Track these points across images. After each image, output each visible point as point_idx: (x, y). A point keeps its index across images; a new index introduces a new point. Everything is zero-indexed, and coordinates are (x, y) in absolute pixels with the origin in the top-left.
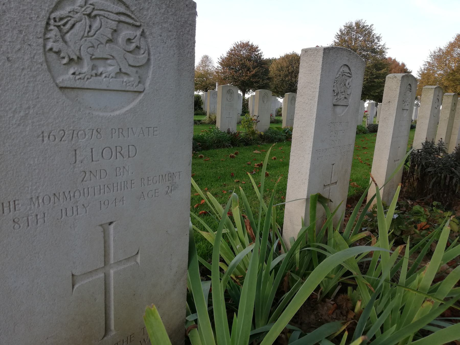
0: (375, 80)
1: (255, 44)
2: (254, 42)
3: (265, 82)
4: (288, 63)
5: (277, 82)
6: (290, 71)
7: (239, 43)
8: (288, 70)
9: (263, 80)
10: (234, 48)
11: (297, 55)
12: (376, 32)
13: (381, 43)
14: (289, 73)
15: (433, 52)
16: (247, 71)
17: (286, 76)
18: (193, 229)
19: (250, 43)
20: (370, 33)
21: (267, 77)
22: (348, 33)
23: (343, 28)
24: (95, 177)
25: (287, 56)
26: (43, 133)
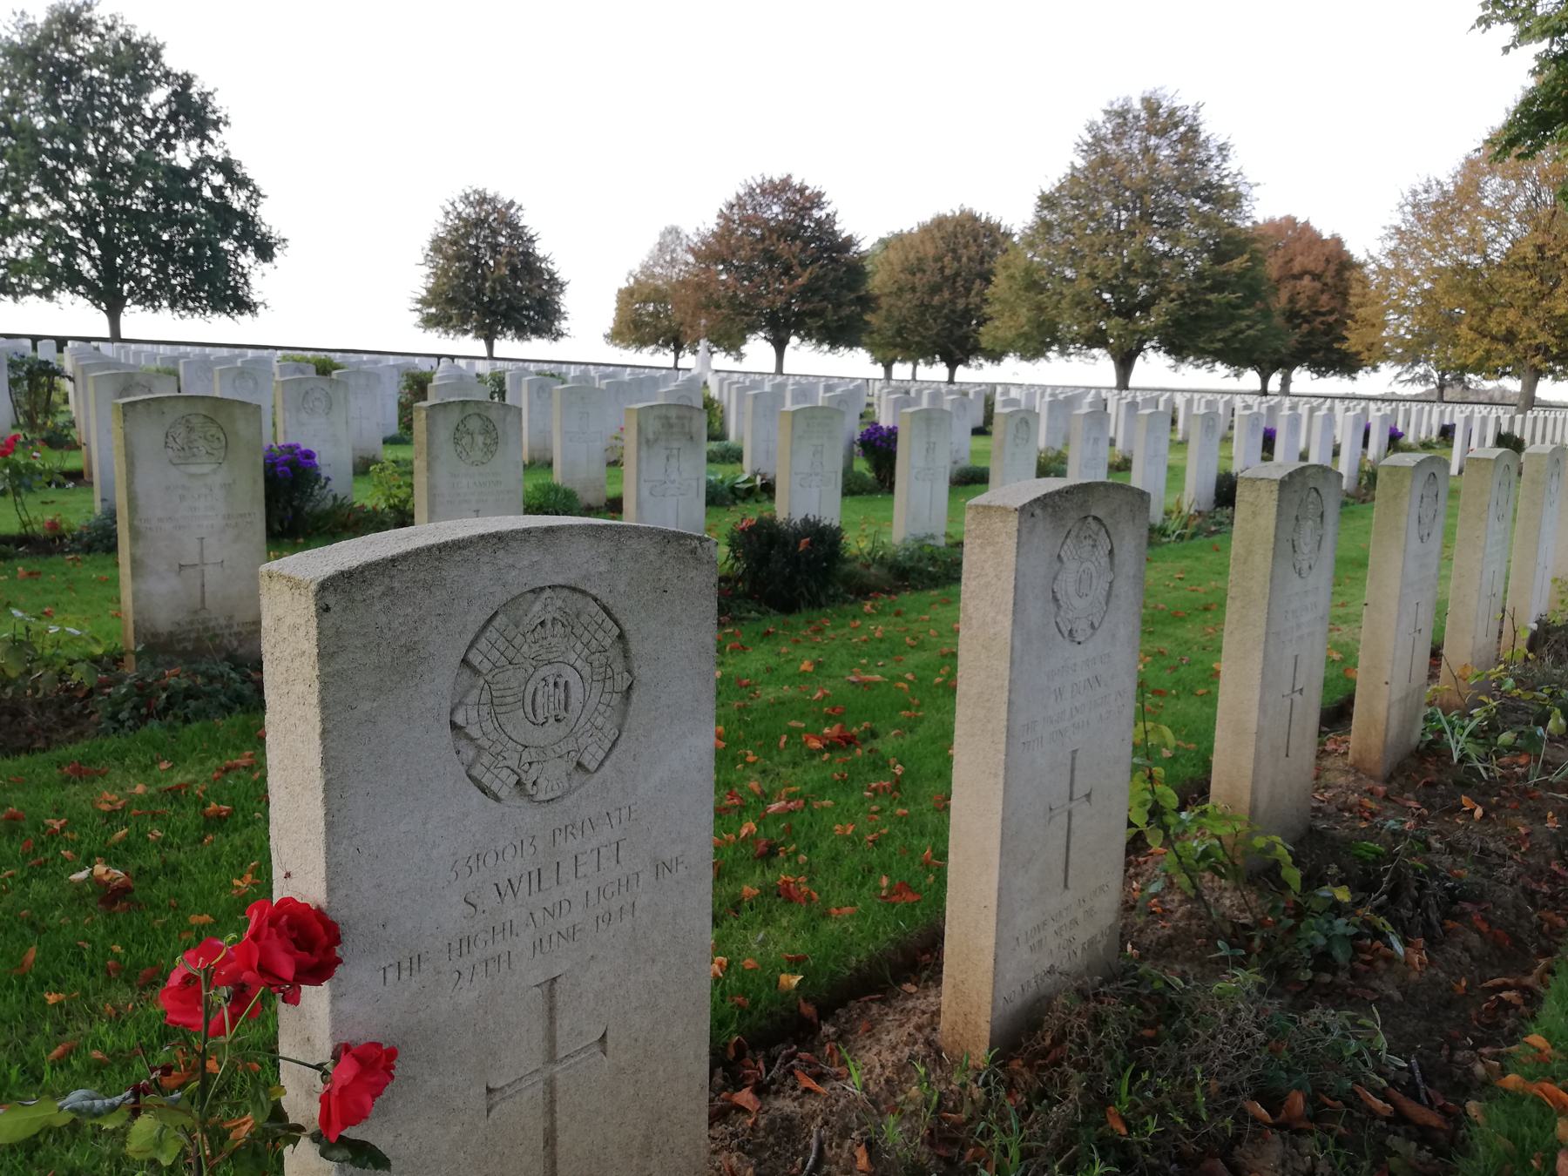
0: (1212, 297)
1: (813, 185)
2: (808, 176)
3: (846, 311)
4: (941, 243)
5: (904, 312)
6: (947, 272)
7: (759, 181)
8: (942, 269)
9: (838, 306)
10: (739, 197)
11: (1336, 266)
12: (1213, 128)
13: (1232, 166)
14: (946, 279)
15: (1407, 194)
17: (935, 289)
20: (1194, 130)
21: (852, 296)
22: (1118, 137)
23: (1100, 118)
25: (940, 222)
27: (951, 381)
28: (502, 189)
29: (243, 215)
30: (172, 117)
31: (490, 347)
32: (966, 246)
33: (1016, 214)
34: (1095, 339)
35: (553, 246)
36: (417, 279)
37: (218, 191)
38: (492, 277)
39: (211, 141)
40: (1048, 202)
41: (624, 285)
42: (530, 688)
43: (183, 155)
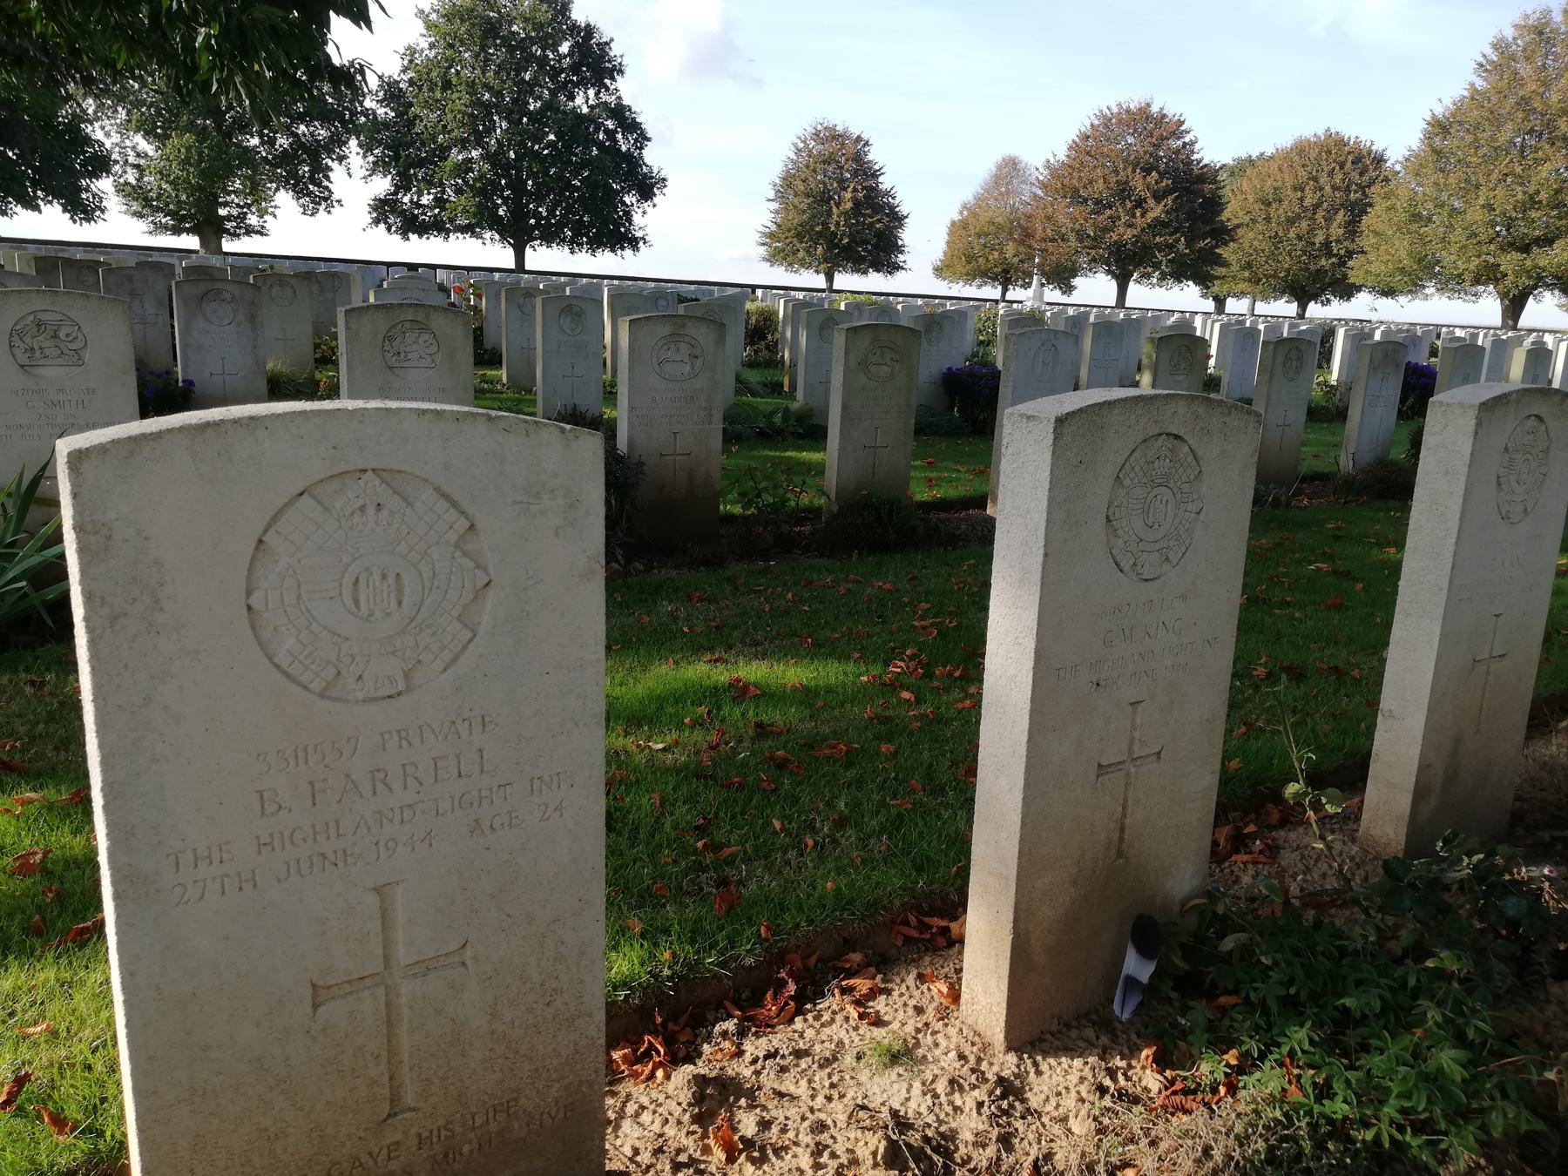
1: (1172, 110)
2: (1169, 103)
7: (1115, 110)
11: (1379, 160)
13: (1509, 33)
14: (1306, 210)
16: (1136, 207)
18: (261, 232)
19: (1155, 109)
23: (1509, 33)
24: (391, 821)
26: (347, 776)
27: (1301, 316)
28: (852, 121)
29: (628, 157)
30: (575, 68)
31: (830, 279)
32: (1331, 173)
33: (1396, 136)
34: (1488, 275)
35: (900, 178)
36: (761, 213)
37: (611, 134)
38: (840, 208)
39: (607, 89)
40: (1440, 127)
41: (957, 217)
42: (348, 581)
43: (583, 101)
